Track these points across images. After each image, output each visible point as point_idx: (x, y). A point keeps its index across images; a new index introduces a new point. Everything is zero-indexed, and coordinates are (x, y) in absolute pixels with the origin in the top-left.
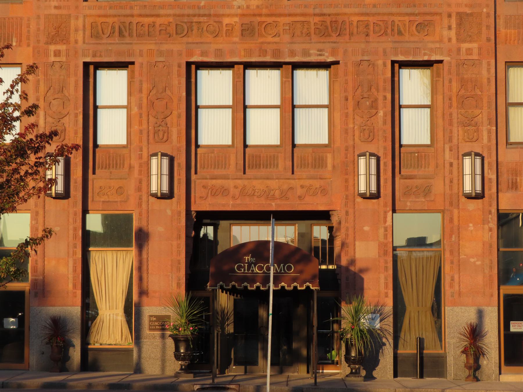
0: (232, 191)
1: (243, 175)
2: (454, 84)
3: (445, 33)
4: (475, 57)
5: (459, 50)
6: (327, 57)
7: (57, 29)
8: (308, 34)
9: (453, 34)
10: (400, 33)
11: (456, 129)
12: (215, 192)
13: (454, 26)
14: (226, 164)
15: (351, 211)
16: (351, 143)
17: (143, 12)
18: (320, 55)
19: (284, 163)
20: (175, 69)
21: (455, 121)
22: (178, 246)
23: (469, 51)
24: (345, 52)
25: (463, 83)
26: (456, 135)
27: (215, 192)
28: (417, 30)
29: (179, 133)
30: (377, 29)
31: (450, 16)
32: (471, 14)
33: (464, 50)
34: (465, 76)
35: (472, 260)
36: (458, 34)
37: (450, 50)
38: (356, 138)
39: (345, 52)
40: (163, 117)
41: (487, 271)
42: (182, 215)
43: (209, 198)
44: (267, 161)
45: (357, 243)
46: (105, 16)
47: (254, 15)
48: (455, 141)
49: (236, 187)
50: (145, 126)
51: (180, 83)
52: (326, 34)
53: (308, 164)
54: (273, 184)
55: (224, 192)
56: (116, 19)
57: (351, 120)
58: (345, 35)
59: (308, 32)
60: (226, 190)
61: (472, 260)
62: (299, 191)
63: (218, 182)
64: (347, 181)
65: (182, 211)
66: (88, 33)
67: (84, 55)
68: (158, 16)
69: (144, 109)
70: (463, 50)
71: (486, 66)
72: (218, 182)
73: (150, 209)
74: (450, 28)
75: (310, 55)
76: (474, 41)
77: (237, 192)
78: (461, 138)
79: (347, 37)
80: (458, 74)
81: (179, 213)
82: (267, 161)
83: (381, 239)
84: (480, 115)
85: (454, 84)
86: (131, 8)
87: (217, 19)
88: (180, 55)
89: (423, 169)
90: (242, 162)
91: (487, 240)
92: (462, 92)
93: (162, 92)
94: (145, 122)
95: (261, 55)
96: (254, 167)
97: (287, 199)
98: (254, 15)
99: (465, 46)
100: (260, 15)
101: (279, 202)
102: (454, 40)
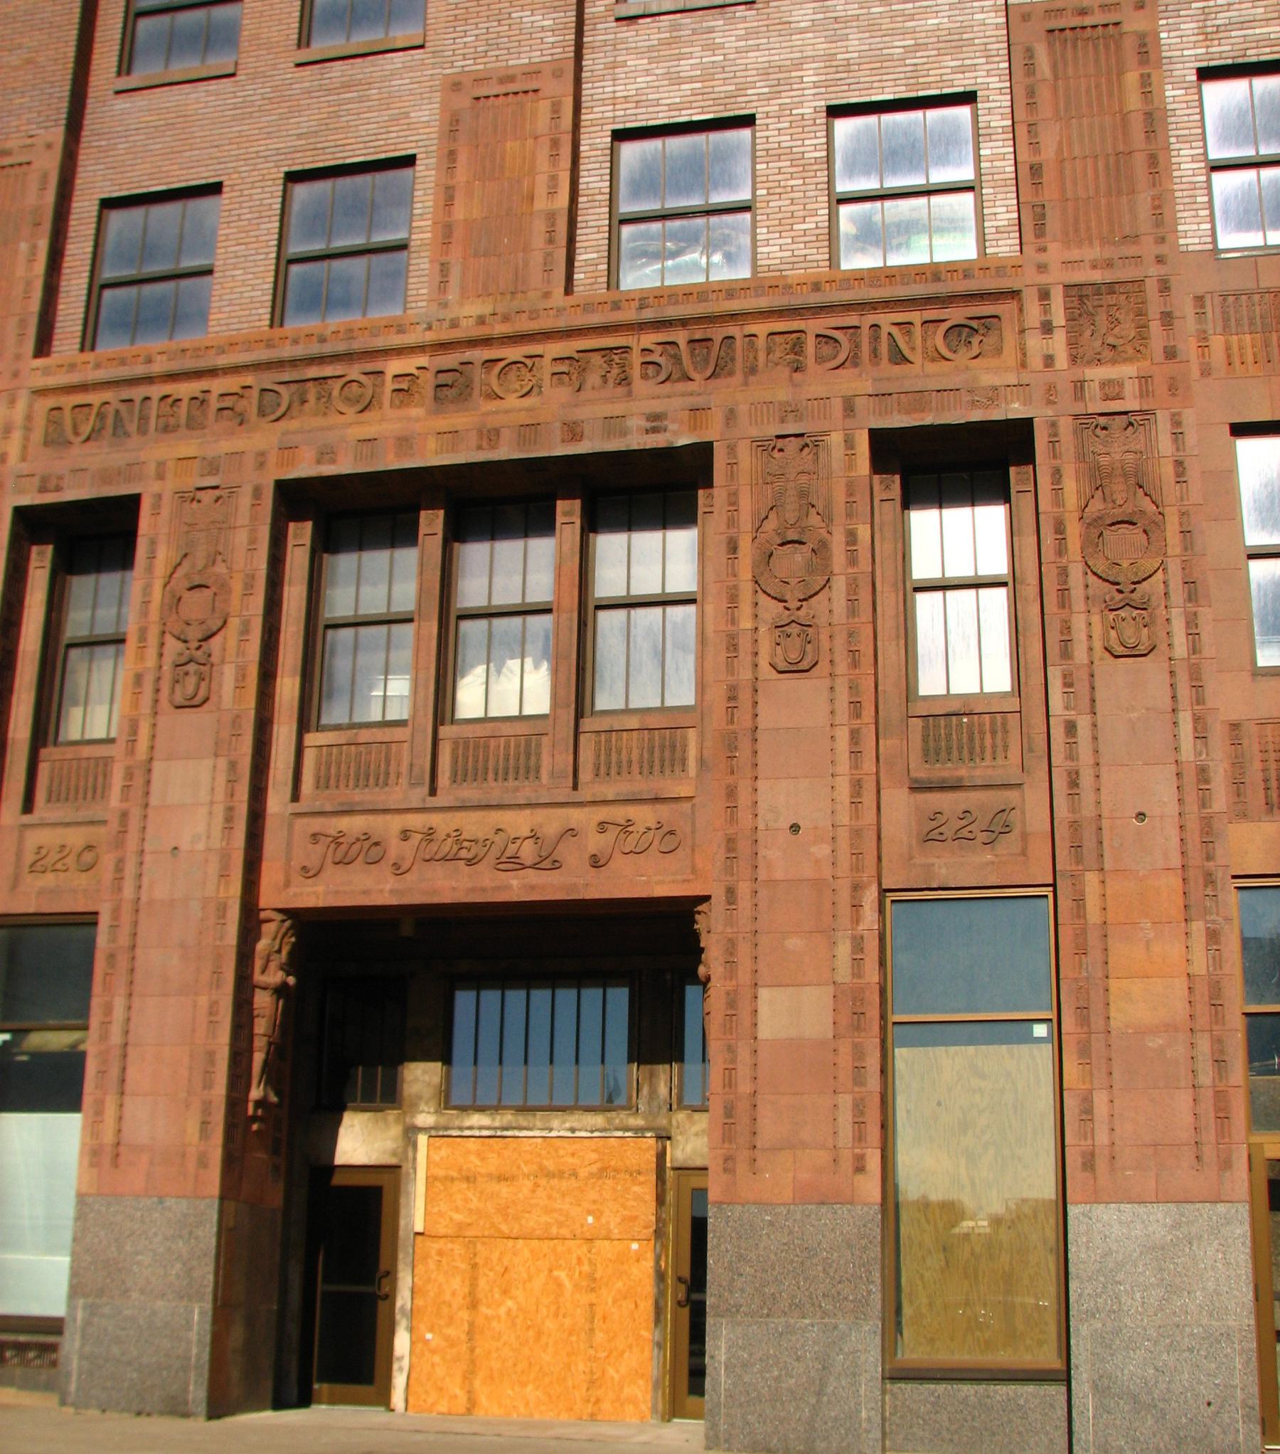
0: (395, 848)
2: (1070, 485)
3: (1034, 342)
4: (1131, 404)
5: (1079, 387)
6: (675, 433)
7: (1160, 1405)
8: (624, 381)
9: (1058, 344)
10: (899, 358)
11: (1083, 617)
12: (348, 852)
13: (1059, 318)
14: (387, 774)
16: (746, 675)
17: (175, 366)
18: (655, 430)
19: (553, 759)
20: (245, 500)
21: (1077, 593)
22: (213, 1010)
23: (1112, 390)
24: (731, 416)
25: (1098, 480)
26: (1083, 637)
27: (348, 852)
28: (948, 346)
29: (241, 676)
30: (827, 350)
31: (1044, 295)
32: (1111, 287)
33: (1096, 386)
34: (1103, 460)
35: (1155, 1042)
36: (1072, 344)
37: (1051, 389)
38: (763, 662)
39: (731, 416)
40: (200, 636)
41: (1206, 1078)
42: (229, 915)
43: (330, 870)
44: (507, 759)
45: (764, 993)
46: (83, 388)
47: (473, 343)
48: (1080, 655)
50: (151, 662)
51: (253, 541)
52: (674, 377)
53: (630, 762)
54: (519, 822)
55: (369, 850)
56: (108, 395)
57: (745, 609)
58: (731, 374)
59: (622, 376)
60: (377, 844)
61: (1155, 1042)
62: (595, 842)
63: (354, 825)
64: (731, 793)
65: (230, 902)
66: (38, 435)
67: (21, 492)
68: (212, 372)
69: (154, 615)
70: (1093, 389)
71: (1169, 426)
72: (354, 825)
73: (144, 898)
74: (1047, 328)
75: (624, 433)
76: (1125, 360)
77: (408, 849)
78: (1098, 645)
79: (738, 378)
80: (1081, 457)
81: (222, 910)
82: (507, 759)
83: (844, 973)
84: (1160, 574)
85: (1070, 485)
86: (149, 361)
87: (370, 367)
88: (261, 465)
89: (988, 762)
91: (1204, 972)
92: (1096, 506)
93: (206, 567)
94: (152, 652)
95: (485, 444)
98: (473, 343)
99: (1096, 374)
100: (487, 342)
101: (532, 876)
102: (1062, 361)
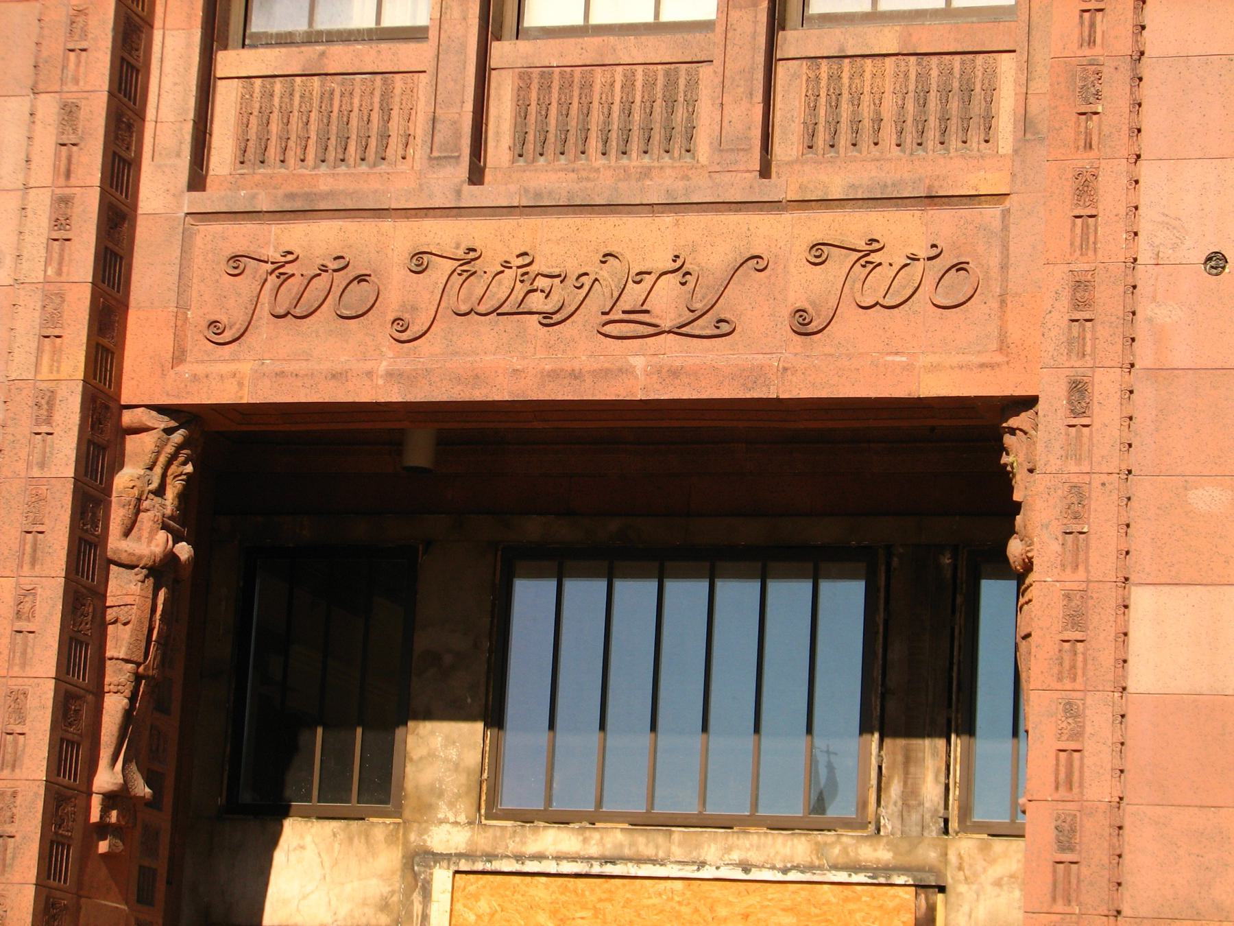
0: (399, 289)
1: (468, 189)
12: (298, 292)
14: (385, 137)
15: (1106, 385)
27: (298, 292)
42: (58, 417)
45: (1142, 598)
49: (419, 262)
54: (648, 241)
55: (347, 289)
60: (361, 279)
62: (804, 285)
63: (314, 239)
64: (1085, 186)
72: (314, 239)
81: (46, 404)
90: (469, 106)
96: (550, 148)
97: (723, 330)
